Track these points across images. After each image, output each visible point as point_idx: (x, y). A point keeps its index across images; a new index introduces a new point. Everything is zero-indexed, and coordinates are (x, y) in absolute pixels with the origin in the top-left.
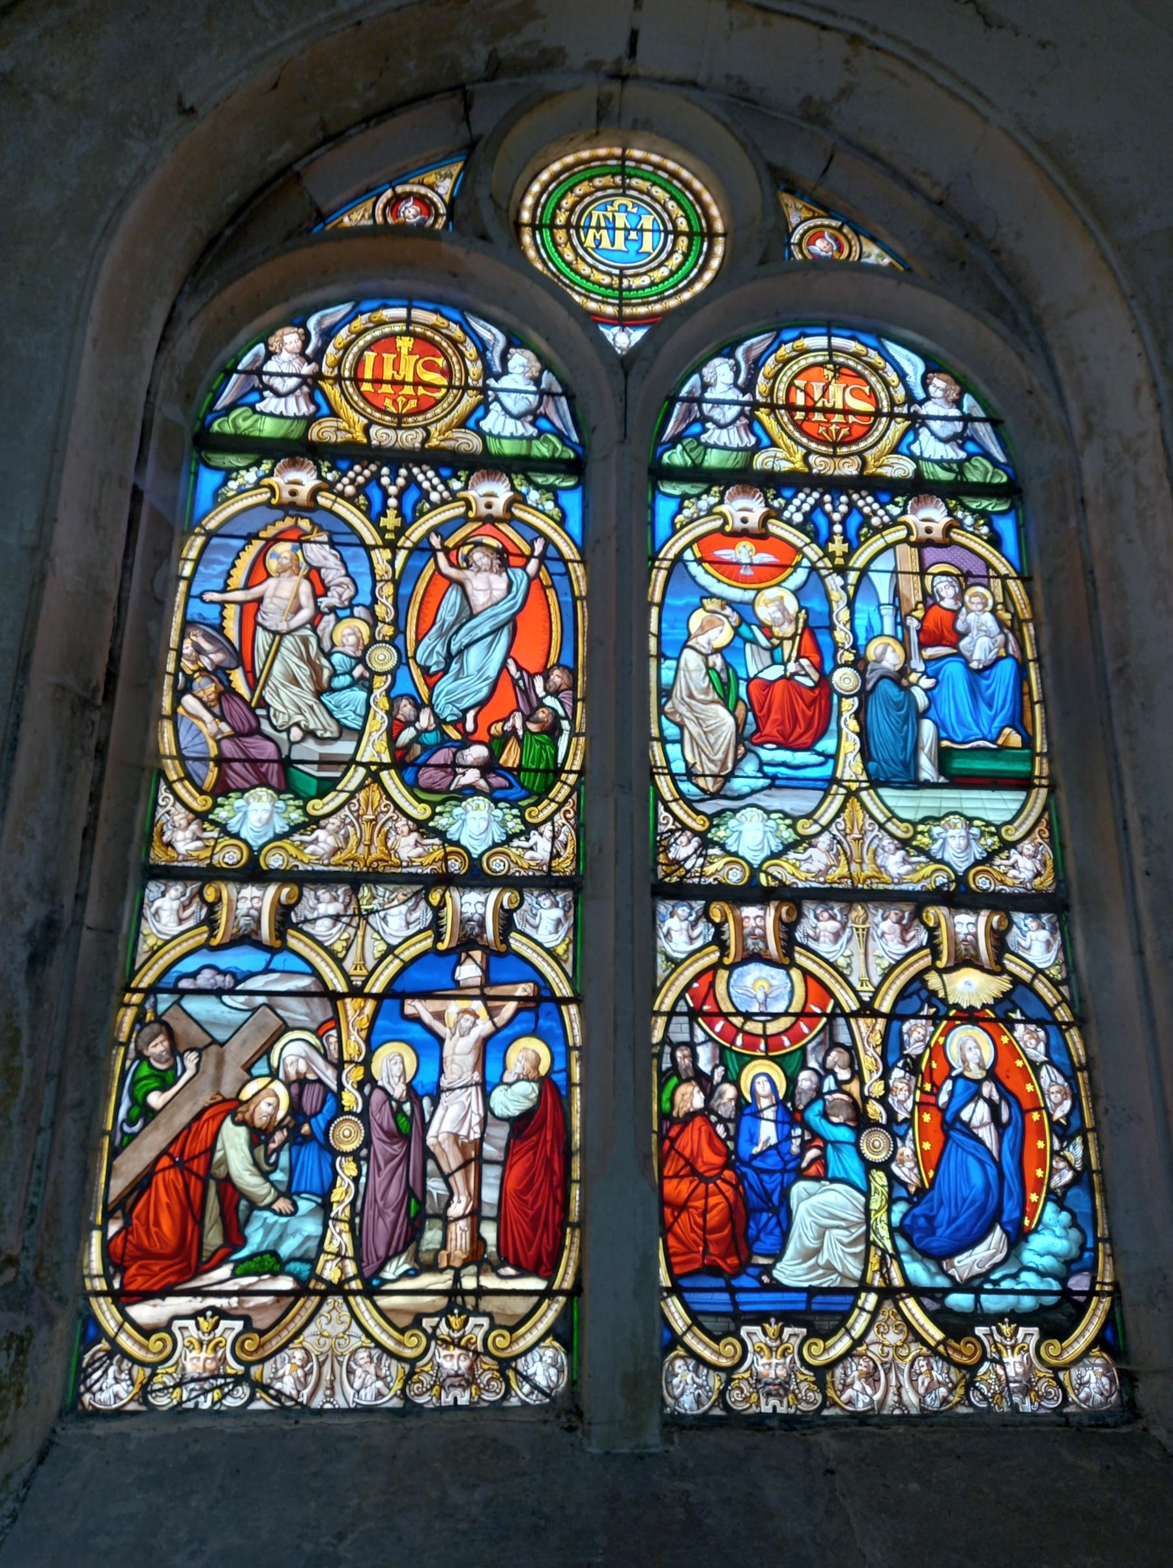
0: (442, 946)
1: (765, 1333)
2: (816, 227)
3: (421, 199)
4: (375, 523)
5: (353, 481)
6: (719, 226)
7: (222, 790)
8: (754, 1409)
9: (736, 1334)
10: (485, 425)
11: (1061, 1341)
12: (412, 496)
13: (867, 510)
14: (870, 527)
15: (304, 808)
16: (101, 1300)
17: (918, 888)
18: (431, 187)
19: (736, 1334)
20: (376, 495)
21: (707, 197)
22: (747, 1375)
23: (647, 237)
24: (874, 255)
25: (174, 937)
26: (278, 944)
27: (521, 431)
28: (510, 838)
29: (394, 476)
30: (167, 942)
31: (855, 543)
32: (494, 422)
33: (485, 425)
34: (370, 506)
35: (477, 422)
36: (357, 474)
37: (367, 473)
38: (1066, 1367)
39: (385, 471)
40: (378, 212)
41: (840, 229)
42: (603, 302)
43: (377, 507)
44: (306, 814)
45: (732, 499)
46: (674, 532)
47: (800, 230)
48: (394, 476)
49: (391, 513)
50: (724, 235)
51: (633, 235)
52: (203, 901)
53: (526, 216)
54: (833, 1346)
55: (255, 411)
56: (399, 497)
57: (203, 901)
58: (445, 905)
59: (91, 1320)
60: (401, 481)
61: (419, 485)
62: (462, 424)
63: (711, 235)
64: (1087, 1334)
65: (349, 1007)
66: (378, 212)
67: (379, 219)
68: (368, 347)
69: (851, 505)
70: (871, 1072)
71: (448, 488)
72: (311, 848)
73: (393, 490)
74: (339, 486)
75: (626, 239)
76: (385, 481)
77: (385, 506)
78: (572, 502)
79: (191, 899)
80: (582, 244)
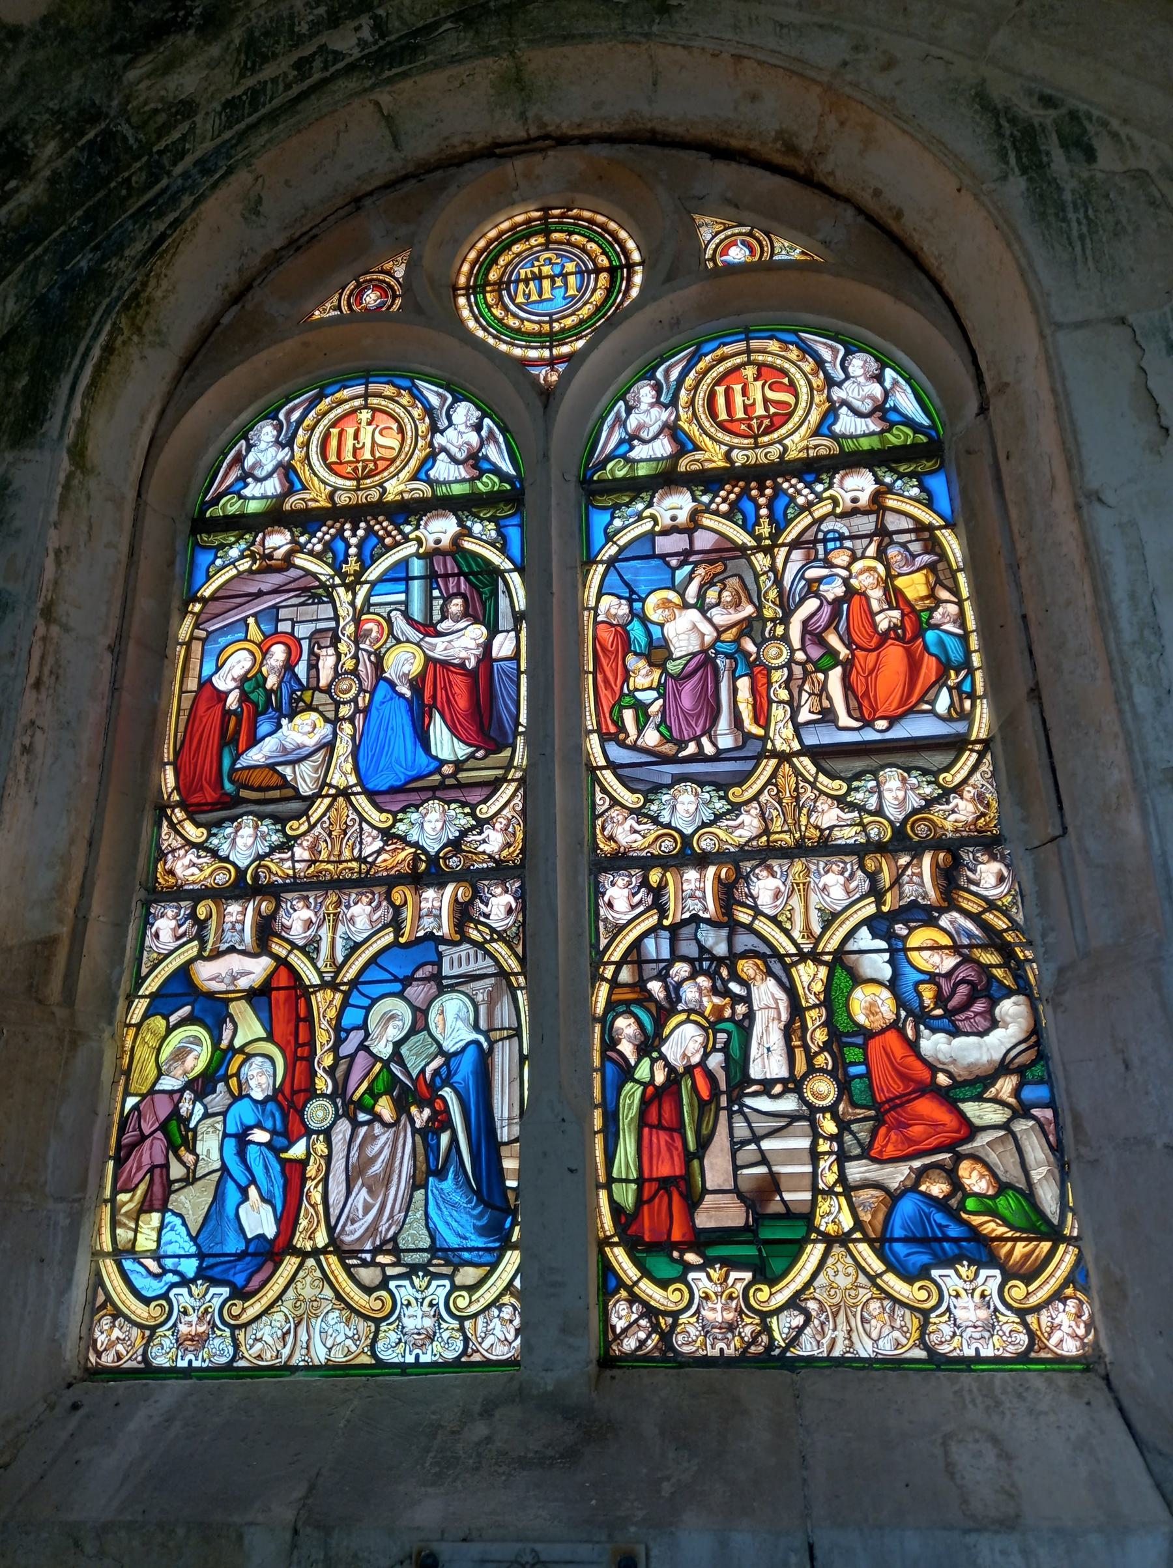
0: (402, 940)
1: (191, 1294)
2: (727, 237)
3: (379, 286)
4: (751, 533)
5: (724, 500)
6: (636, 257)
7: (653, 790)
8: (702, 1353)
9: (683, 1279)
10: (837, 428)
11: (771, 1287)
12: (781, 502)
13: (791, 491)
14: (384, 545)
15: (283, 831)
16: (616, 1250)
17: (851, 841)
18: (388, 273)
19: (683, 1279)
20: (340, 545)
21: (623, 234)
22: (694, 1320)
23: (572, 279)
24: (787, 251)
25: (172, 952)
26: (458, 937)
27: (464, 474)
28: (718, 817)
29: (761, 489)
30: (167, 956)
31: (782, 526)
32: (443, 469)
33: (837, 428)
34: (745, 520)
35: (829, 428)
36: (325, 534)
37: (737, 490)
38: (1037, 1309)
39: (347, 526)
40: (344, 303)
41: (750, 234)
42: (527, 347)
43: (752, 519)
44: (940, 786)
45: (660, 500)
46: (209, 578)
47: (712, 246)
48: (761, 489)
49: (352, 560)
50: (641, 264)
51: (559, 282)
52: (391, 903)
53: (462, 280)
54: (478, 1300)
55: (240, 497)
56: (360, 546)
57: (391, 903)
58: (667, 884)
59: (607, 1268)
60: (360, 533)
61: (376, 533)
62: (816, 433)
63: (630, 266)
64: (1058, 1274)
65: (802, 972)
66: (344, 303)
67: (345, 309)
68: (718, 382)
69: (370, 530)
70: (322, 1045)
71: (813, 492)
72: (738, 832)
73: (353, 541)
74: (309, 546)
75: (553, 288)
76: (347, 534)
77: (758, 517)
78: (937, 483)
79: (640, 888)
80: (513, 300)
